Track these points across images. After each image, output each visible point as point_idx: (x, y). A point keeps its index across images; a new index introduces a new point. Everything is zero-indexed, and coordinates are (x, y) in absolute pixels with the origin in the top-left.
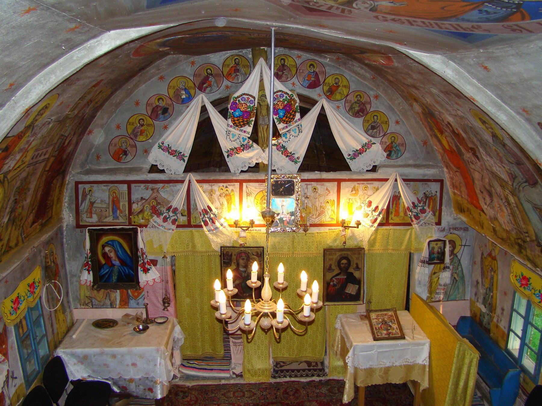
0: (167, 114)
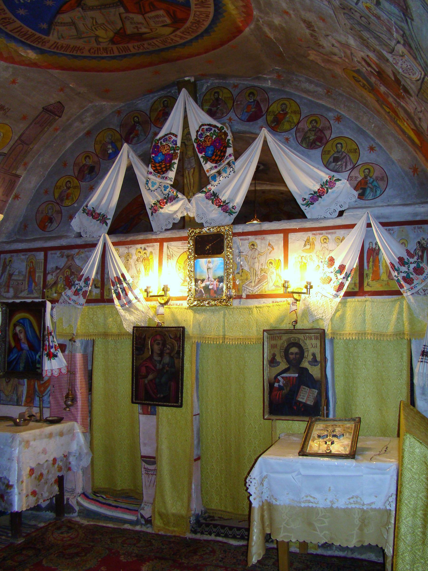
0: (94, 173)
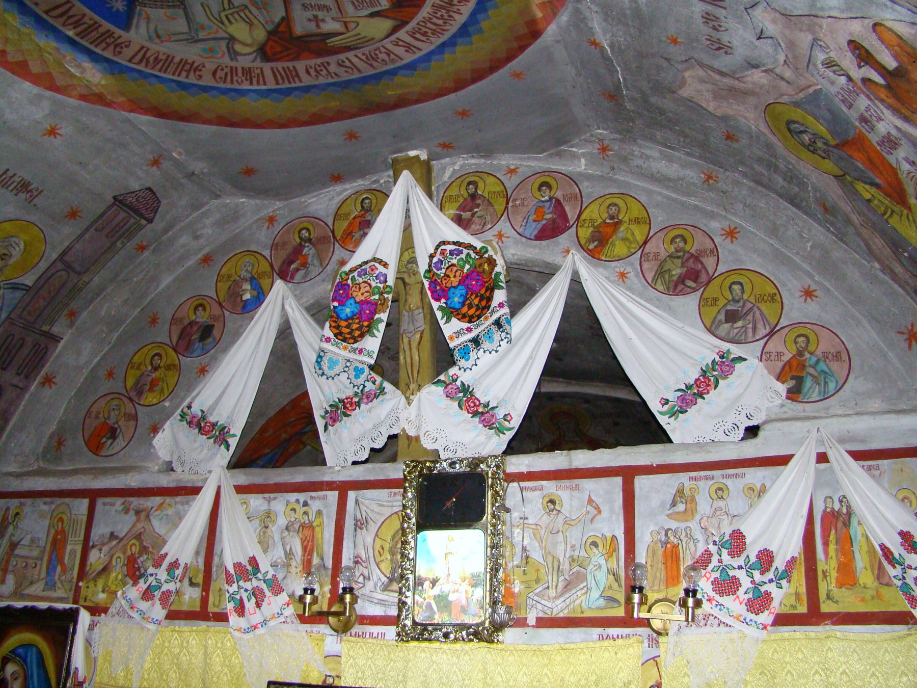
0: (210, 340)
